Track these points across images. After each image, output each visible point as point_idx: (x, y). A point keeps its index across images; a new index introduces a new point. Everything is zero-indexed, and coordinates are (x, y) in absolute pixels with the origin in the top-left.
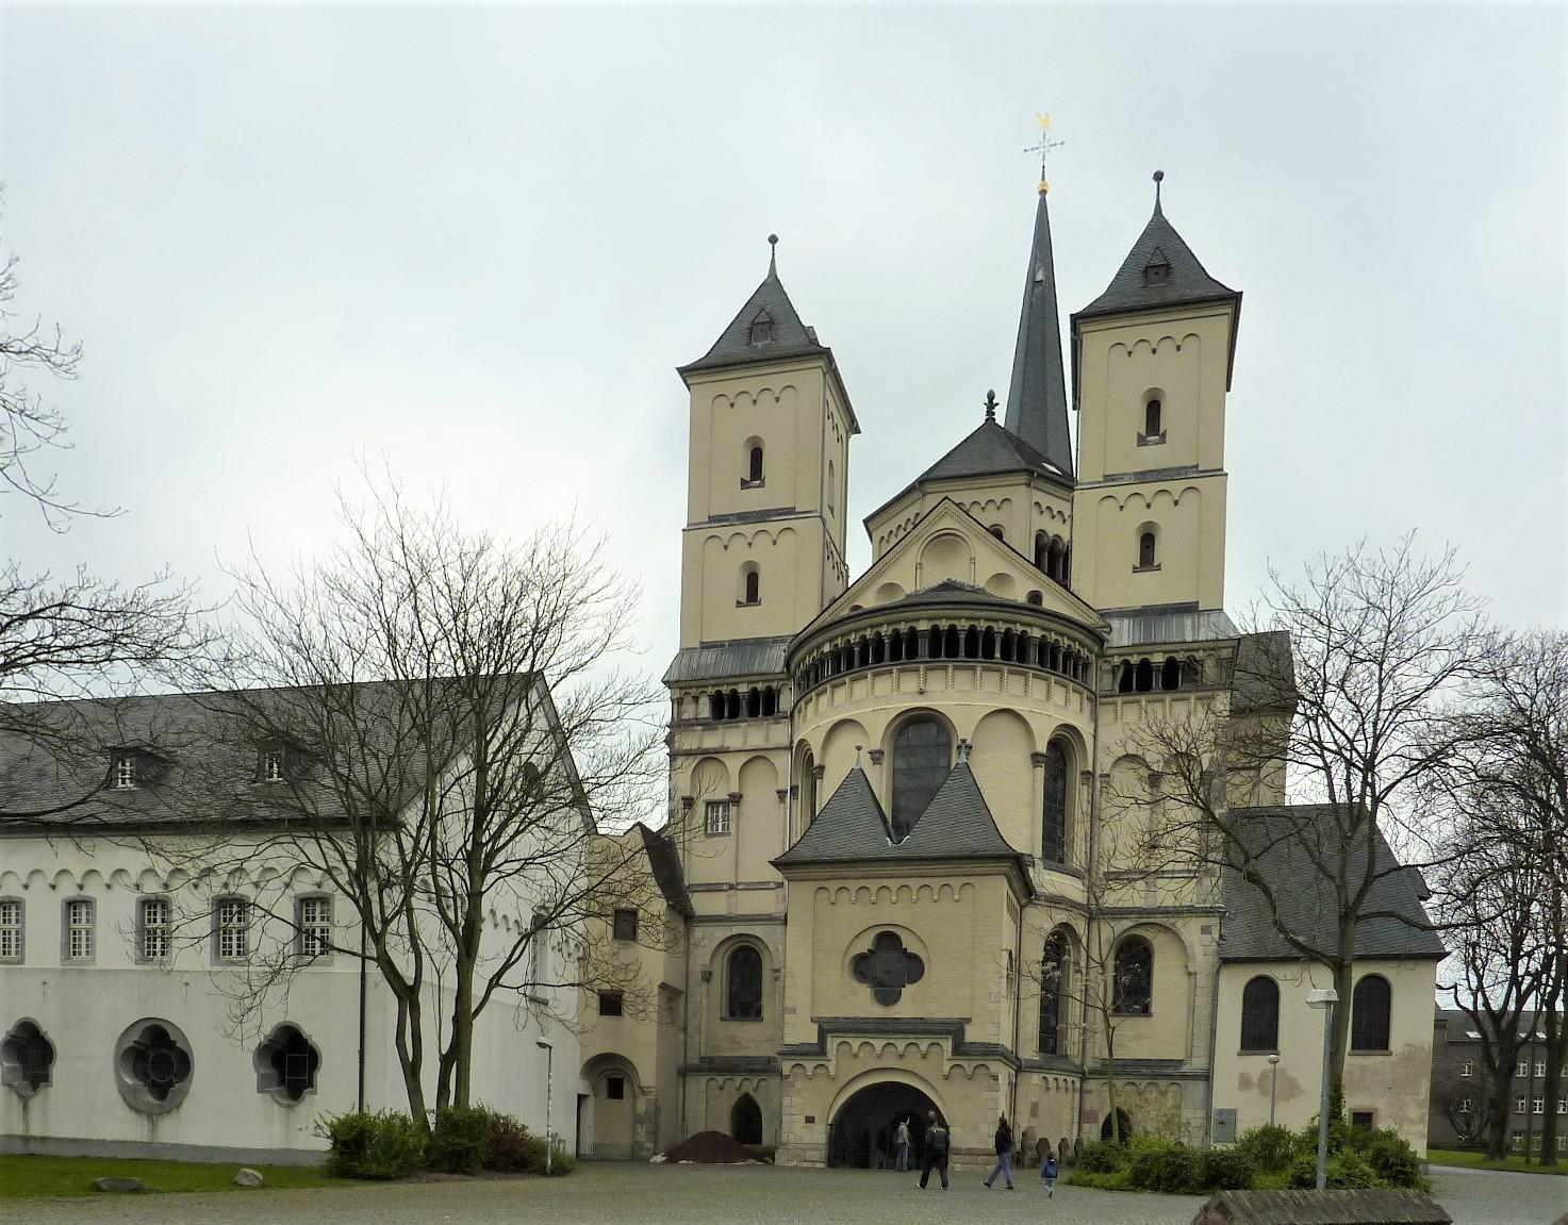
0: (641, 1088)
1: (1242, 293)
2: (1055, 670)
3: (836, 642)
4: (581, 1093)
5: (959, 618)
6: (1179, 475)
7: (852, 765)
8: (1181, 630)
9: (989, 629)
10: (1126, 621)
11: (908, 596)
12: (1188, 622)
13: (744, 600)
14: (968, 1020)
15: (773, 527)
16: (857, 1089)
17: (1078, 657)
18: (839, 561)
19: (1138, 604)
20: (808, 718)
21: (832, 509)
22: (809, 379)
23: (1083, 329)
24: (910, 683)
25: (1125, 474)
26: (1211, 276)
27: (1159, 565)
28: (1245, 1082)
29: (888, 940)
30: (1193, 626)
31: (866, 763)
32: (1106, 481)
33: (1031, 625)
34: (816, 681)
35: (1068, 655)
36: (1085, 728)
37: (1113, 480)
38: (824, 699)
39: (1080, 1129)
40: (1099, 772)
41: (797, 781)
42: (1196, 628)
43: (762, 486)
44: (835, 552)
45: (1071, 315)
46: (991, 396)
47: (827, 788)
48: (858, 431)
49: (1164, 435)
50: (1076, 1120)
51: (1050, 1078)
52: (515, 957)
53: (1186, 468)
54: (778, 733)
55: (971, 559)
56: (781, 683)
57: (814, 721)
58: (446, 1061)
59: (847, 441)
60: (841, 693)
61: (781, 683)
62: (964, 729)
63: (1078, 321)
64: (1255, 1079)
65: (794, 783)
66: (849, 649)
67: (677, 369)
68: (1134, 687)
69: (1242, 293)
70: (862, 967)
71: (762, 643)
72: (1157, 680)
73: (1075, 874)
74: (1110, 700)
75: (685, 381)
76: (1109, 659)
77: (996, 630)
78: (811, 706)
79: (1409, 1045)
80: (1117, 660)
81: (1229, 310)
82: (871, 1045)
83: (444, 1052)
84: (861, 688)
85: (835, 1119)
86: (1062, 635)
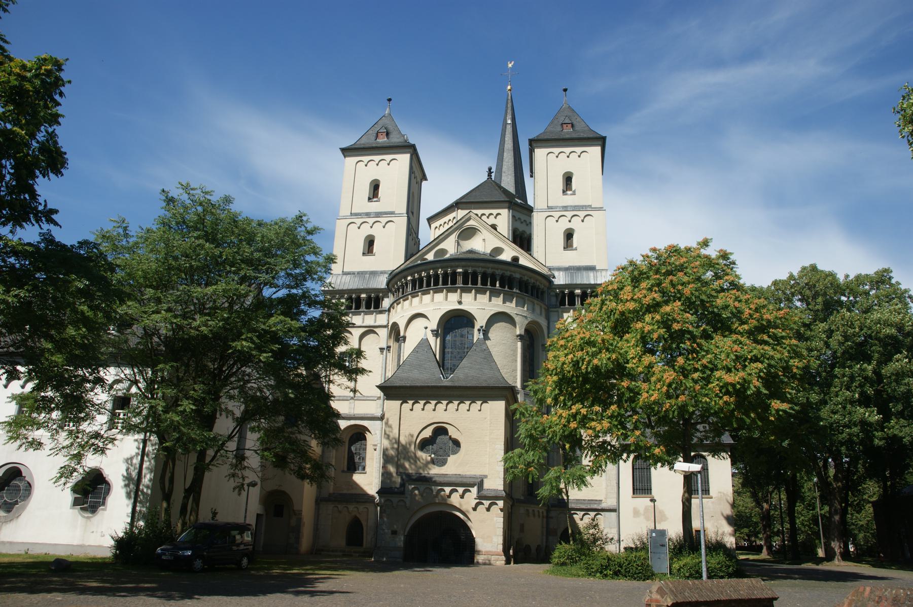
0: (293, 510)
5: (479, 267)
8: (588, 277)
10: (561, 273)
11: (451, 255)
12: (591, 274)
14: (486, 476)
15: (384, 220)
16: (424, 514)
17: (538, 289)
19: (567, 265)
21: (413, 213)
22: (404, 159)
24: (454, 297)
27: (576, 248)
28: (636, 513)
29: (440, 431)
30: (594, 277)
32: (549, 209)
33: (515, 272)
34: (403, 294)
35: (534, 287)
36: (543, 322)
38: (407, 302)
39: (547, 539)
42: (596, 278)
43: (378, 201)
46: (490, 169)
47: (408, 348)
48: (426, 179)
49: (574, 191)
50: (545, 534)
52: (234, 434)
54: (382, 319)
57: (401, 313)
58: (188, 492)
60: (416, 300)
62: (481, 321)
64: (642, 510)
65: (389, 344)
75: (343, 154)
79: (720, 492)
81: (600, 143)
82: (391, 500)
83: (186, 488)
84: (427, 298)
85: (409, 532)
86: (531, 278)
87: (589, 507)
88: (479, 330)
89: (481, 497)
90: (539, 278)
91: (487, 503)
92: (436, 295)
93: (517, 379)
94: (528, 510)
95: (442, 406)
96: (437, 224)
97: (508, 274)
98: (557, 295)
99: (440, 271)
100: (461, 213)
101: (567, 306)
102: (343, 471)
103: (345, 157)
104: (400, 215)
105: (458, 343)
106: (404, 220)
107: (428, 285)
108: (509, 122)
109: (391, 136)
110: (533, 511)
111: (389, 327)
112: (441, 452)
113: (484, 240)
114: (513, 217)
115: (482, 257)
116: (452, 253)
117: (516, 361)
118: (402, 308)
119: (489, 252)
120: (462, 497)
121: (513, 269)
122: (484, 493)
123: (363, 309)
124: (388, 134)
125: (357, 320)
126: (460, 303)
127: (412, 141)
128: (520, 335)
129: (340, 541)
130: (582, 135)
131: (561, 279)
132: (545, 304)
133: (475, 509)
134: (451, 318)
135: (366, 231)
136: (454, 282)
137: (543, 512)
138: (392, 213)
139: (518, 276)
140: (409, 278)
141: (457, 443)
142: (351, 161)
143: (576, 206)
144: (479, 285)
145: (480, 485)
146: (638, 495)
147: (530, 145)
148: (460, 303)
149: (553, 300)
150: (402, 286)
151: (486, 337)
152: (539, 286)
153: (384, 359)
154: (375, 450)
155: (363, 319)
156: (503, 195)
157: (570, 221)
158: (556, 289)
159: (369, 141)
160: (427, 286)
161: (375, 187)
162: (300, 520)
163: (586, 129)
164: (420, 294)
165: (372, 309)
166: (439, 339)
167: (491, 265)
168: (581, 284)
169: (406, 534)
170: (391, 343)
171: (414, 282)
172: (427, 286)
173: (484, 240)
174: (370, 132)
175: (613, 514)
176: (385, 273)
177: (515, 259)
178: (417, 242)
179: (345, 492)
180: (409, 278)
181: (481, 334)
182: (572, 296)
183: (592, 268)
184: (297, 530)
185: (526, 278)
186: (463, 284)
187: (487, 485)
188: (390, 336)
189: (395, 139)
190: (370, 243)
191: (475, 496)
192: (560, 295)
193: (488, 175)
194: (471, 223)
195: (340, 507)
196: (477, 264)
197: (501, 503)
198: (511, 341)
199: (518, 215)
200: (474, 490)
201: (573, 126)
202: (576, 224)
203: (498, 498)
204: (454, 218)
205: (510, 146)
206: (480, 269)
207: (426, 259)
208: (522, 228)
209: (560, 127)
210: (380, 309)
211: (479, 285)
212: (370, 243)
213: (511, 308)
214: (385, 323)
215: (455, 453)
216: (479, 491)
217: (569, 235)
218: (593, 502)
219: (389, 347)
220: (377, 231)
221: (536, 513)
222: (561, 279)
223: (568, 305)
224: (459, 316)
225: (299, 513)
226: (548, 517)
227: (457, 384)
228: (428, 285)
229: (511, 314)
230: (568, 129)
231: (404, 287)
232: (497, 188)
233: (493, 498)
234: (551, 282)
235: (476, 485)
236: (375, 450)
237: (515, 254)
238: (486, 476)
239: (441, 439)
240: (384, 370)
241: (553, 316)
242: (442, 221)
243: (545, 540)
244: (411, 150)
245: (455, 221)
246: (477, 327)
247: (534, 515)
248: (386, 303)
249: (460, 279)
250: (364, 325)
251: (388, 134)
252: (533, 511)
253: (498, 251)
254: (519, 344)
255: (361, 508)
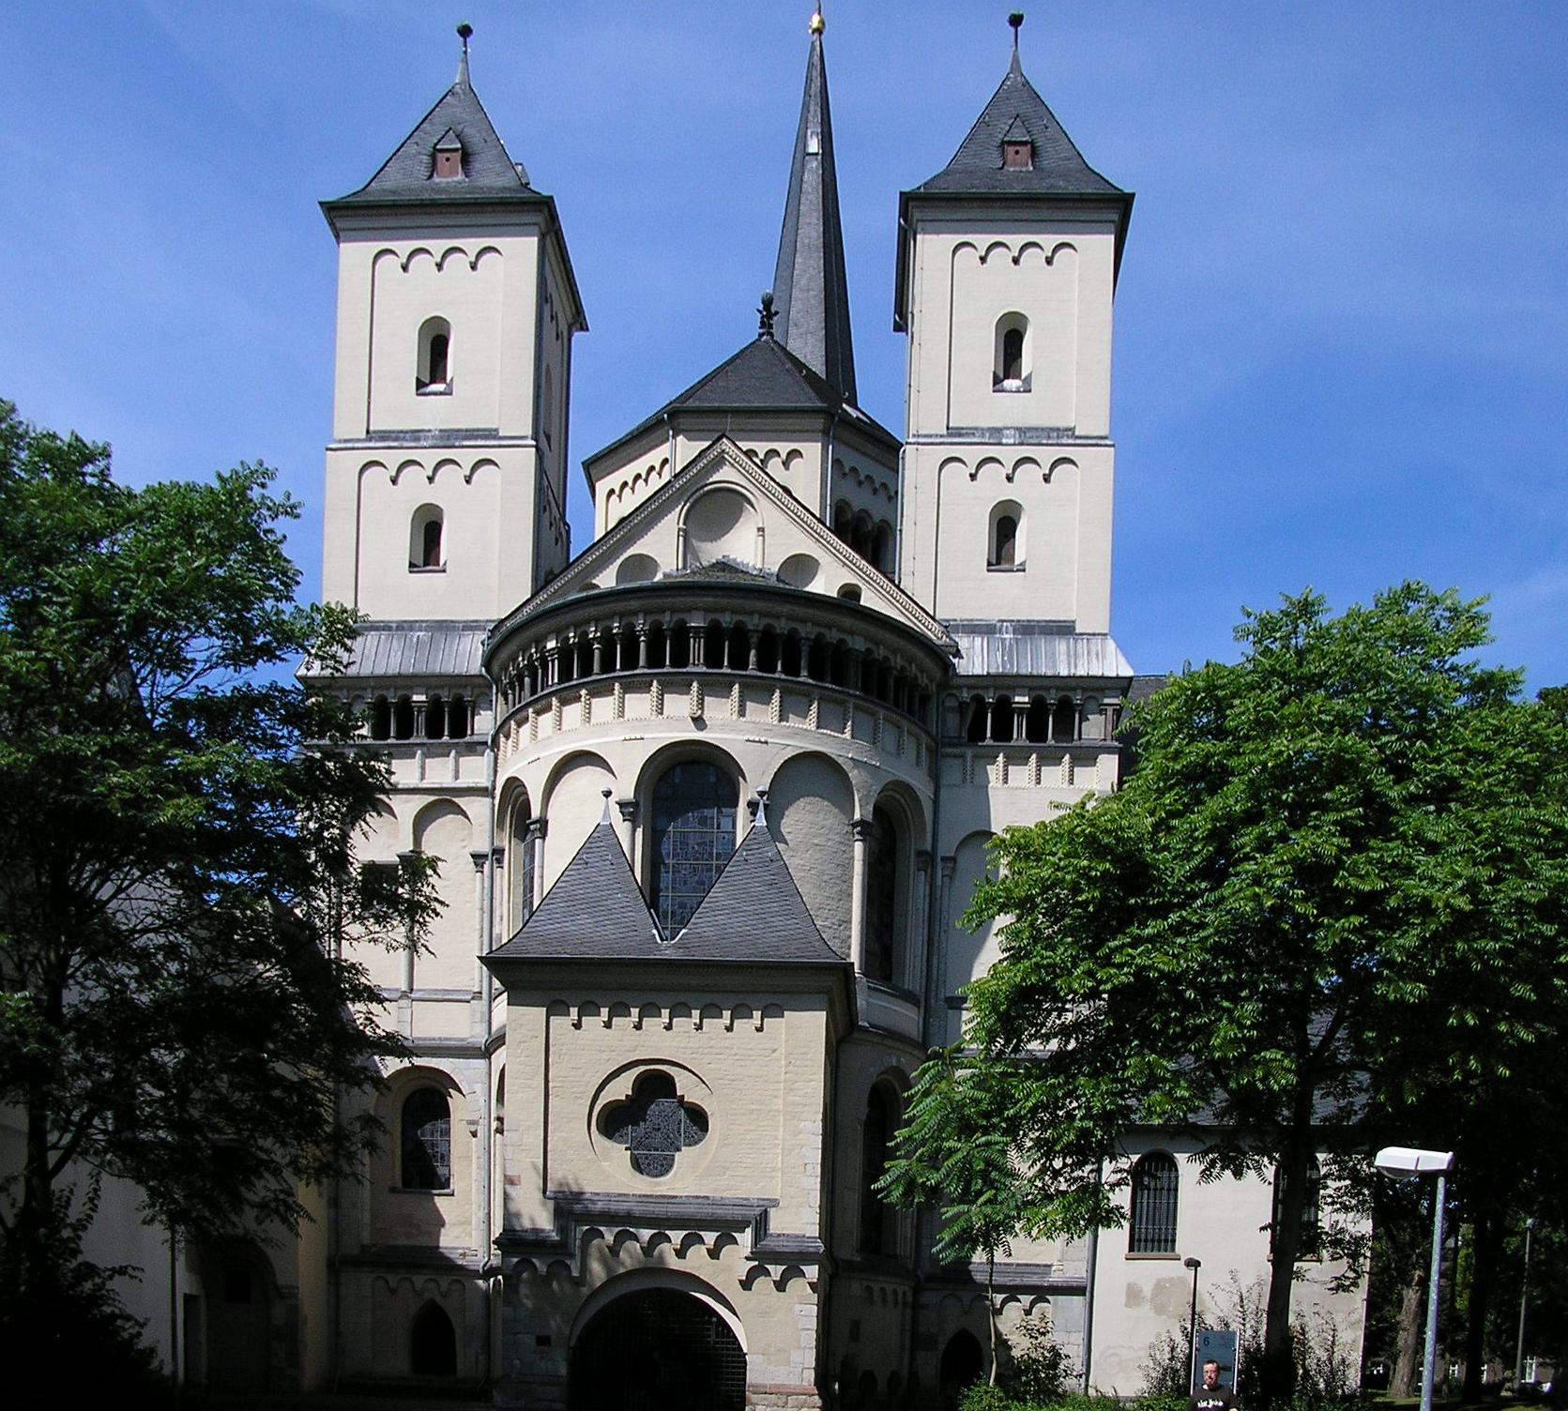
1: (1133, 195)
2: (884, 701)
3: (632, 619)
4: (187, 1292)
6: (1049, 437)
7: (598, 819)
8: (1052, 657)
9: (793, 632)
10: (978, 640)
12: (1061, 646)
13: (421, 562)
17: (914, 686)
18: (558, 516)
20: (521, 747)
21: (548, 438)
23: (917, 215)
24: (680, 705)
25: (976, 429)
26: (1090, 165)
27: (1022, 564)
28: (1133, 1296)
31: (616, 818)
32: (950, 435)
33: (852, 633)
34: (534, 692)
36: (923, 788)
37: (960, 435)
38: (547, 719)
39: (913, 1358)
40: (941, 853)
41: (501, 841)
42: (1073, 657)
43: (448, 393)
44: (553, 504)
45: (901, 193)
47: (556, 854)
48: (584, 328)
49: (1027, 381)
51: (876, 1287)
53: (1058, 429)
54: (475, 770)
55: (759, 529)
56: (476, 691)
59: (569, 340)
60: (573, 712)
61: (476, 691)
63: (911, 204)
66: (585, 648)
67: (321, 203)
68: (989, 735)
69: (1133, 195)
70: (613, 1121)
71: (448, 629)
72: (1020, 726)
73: (909, 997)
74: (956, 751)
75: (332, 224)
76: (954, 692)
77: (803, 635)
78: (526, 728)
80: (965, 695)
81: (1115, 217)
84: (604, 707)
86: (894, 652)
87: (1018, 1281)
88: (753, 806)
89: (762, 1257)
90: (920, 654)
91: (776, 1271)
92: (631, 699)
93: (849, 948)
94: (869, 1289)
95: (654, 1025)
96: (613, 480)
97: (833, 636)
98: (962, 707)
99: (640, 624)
100: (683, 450)
101: (989, 742)
102: (393, 1190)
103: (337, 237)
104: (513, 442)
105: (691, 842)
106: (525, 460)
107: (608, 665)
108: (814, 146)
109: (476, 165)
110: (883, 1290)
111: (498, 792)
112: (657, 1139)
113: (761, 530)
114: (836, 462)
115: (749, 581)
116: (668, 571)
117: (850, 895)
118: (535, 735)
119: (775, 569)
120: (714, 1254)
121: (848, 622)
122: (768, 1243)
123: (419, 738)
124: (466, 158)
125: (405, 772)
126: (699, 722)
127: (540, 186)
128: (862, 823)
129: (397, 1362)
130: (1063, 186)
131: (978, 661)
132: (928, 734)
133: (746, 1285)
134: (672, 769)
135: (416, 490)
136: (680, 659)
137: (904, 1294)
138: (491, 434)
139: (858, 644)
140: (551, 644)
141: (698, 1118)
142: (355, 254)
143: (1029, 429)
144: (752, 670)
145: (761, 1224)
146: (1141, 1254)
147: (904, 213)
148: (699, 722)
149: (953, 721)
150: (531, 667)
151: (774, 832)
152: (915, 678)
153: (487, 884)
154: (474, 1134)
155: (423, 768)
156: (808, 389)
157: (1009, 479)
158: (959, 688)
159: (408, 179)
160: (603, 671)
161: (436, 344)
162: (294, 1311)
163: (1074, 164)
164: (583, 692)
165: (446, 738)
166: (639, 831)
167: (786, 608)
168: (1032, 676)
169: (572, 1344)
170: (504, 841)
171: (564, 653)
172: (603, 671)
173: (761, 530)
174: (411, 148)
175: (1078, 1301)
176: (477, 628)
177: (851, 593)
178: (563, 538)
179: (402, 1241)
180: (551, 644)
181: (761, 814)
182: (1004, 711)
183: (1064, 629)
184: (290, 1334)
185: (881, 652)
186: (707, 664)
187: (776, 1224)
188: (498, 823)
189: (490, 179)
190: (429, 530)
191: (747, 1252)
192: (973, 707)
193: (763, 325)
194: (726, 474)
195: (393, 1280)
196: (749, 604)
197: (812, 1272)
198: (837, 838)
199: (851, 459)
200: (745, 1238)
201: (1034, 153)
202: (1026, 488)
203: (807, 1258)
204: (665, 461)
205: (814, 234)
206: (756, 618)
207: (596, 587)
208: (860, 500)
209: (996, 154)
210: (467, 739)
211: (752, 670)
212: (429, 530)
213: (840, 744)
214: (484, 782)
215: (692, 1142)
216: (757, 1238)
217: (1005, 524)
218: (1028, 1269)
219: (498, 852)
220: (448, 493)
221: (890, 1297)
222: (978, 661)
223: (994, 737)
224: (693, 762)
225: (289, 1294)
226: (916, 1306)
227: (697, 956)
228: (608, 665)
229: (840, 761)
230: (1019, 164)
231: (535, 670)
232: (789, 365)
233: (793, 1262)
234: (949, 667)
235: (747, 1224)
236: (474, 1134)
237: (850, 578)
238: (775, 1203)
239: (660, 1107)
240: (486, 916)
241: (951, 773)
242: (627, 473)
243: (906, 1361)
244: (539, 218)
245: (666, 476)
246: (747, 793)
247: (884, 1301)
248: (484, 723)
249: (697, 648)
250: (425, 785)
251: (466, 158)
252: (883, 1290)
253: (801, 565)
254: (858, 847)
255: (445, 1282)
